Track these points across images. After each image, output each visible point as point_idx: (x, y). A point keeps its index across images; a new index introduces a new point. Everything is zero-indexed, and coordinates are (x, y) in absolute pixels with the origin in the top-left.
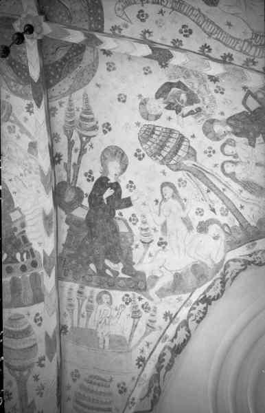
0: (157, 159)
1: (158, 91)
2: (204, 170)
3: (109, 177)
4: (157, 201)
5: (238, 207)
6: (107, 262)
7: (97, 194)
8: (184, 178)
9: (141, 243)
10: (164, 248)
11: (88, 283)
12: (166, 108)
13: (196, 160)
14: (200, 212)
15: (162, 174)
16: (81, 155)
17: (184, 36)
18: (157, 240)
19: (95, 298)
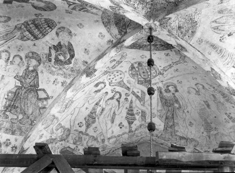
12: (60, 43)
16: (94, 102)
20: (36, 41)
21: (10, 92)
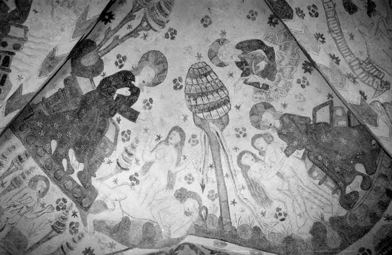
0: (189, 101)
1: (244, 42)
2: (222, 144)
3: (137, 78)
4: (159, 138)
5: (230, 200)
6: (71, 153)
7: (114, 83)
8: (198, 138)
9: (116, 163)
10: (133, 185)
11: (37, 156)
12: (237, 63)
13: (222, 130)
14: (189, 179)
15: (183, 117)
16: (129, 35)
17: (310, 13)
18: (131, 172)
19: (29, 177)
20: (231, 103)
21: (310, 172)
